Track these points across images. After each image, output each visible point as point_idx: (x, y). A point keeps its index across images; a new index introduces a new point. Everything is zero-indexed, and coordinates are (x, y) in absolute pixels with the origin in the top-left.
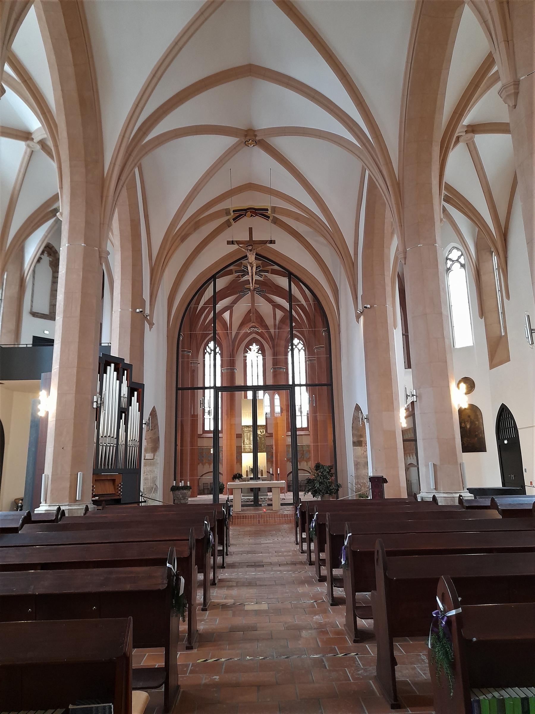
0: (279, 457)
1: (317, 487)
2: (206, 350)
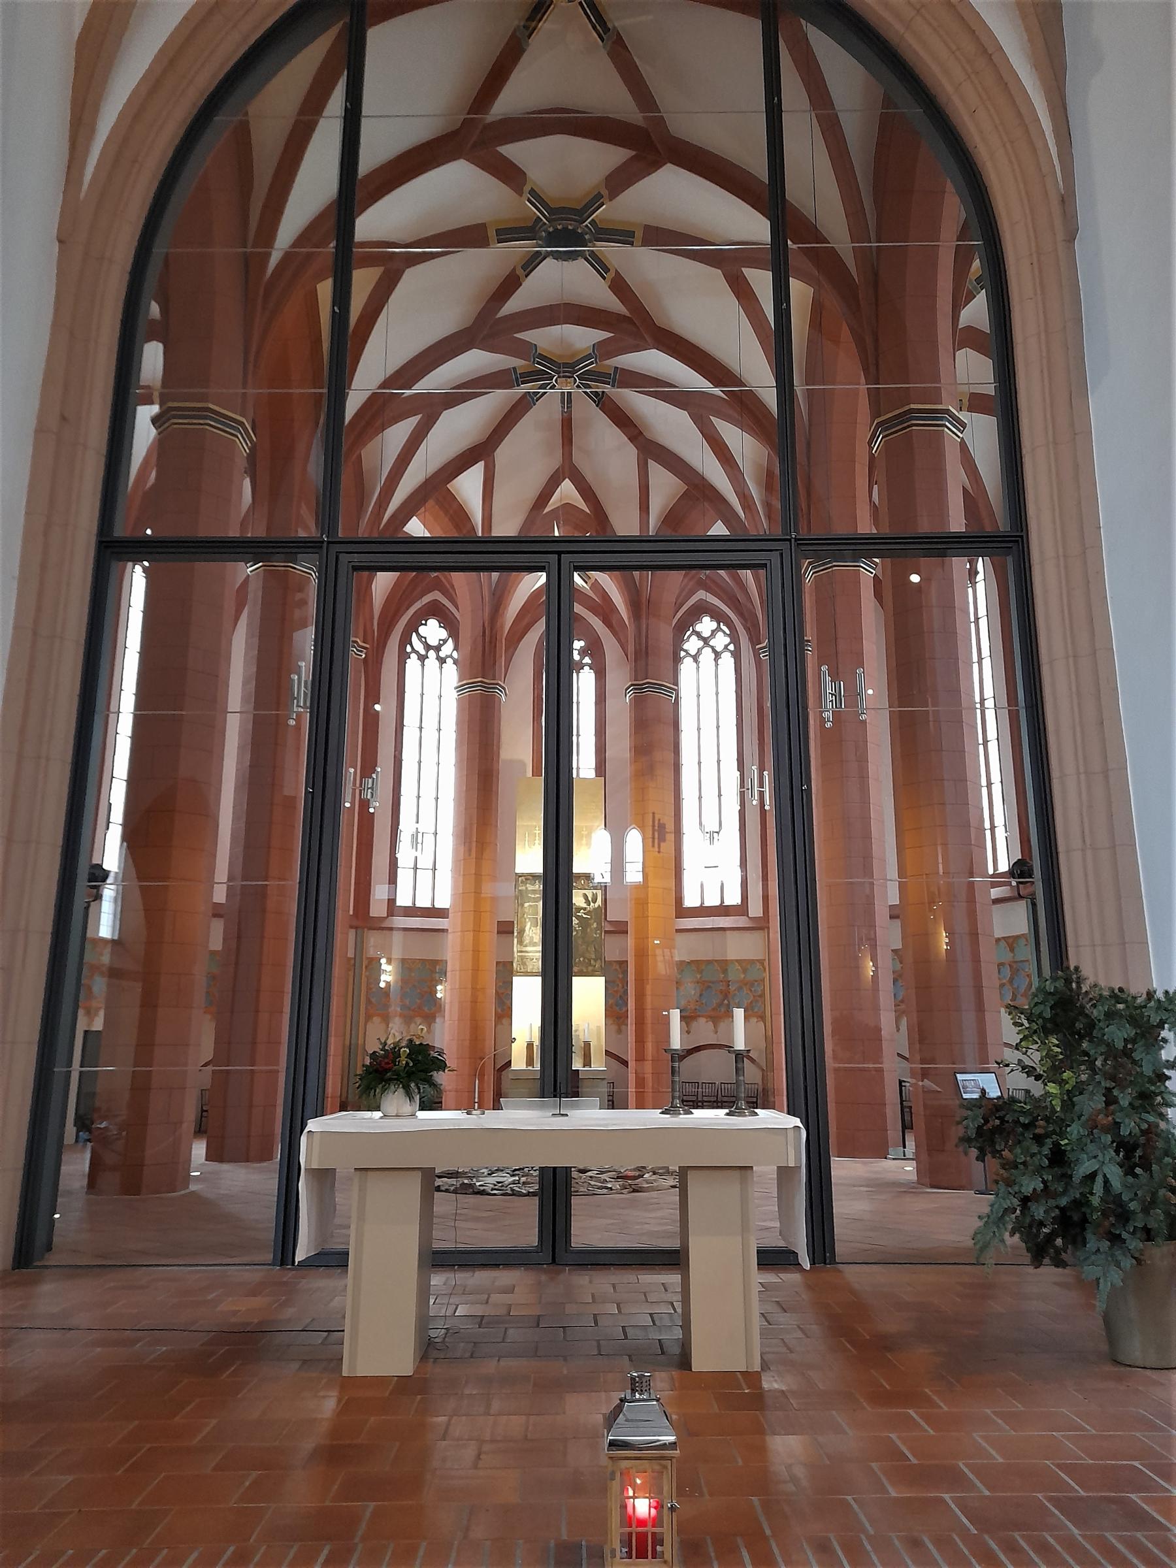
0: (649, 999)
1: (1099, 1180)
2: (408, 646)
